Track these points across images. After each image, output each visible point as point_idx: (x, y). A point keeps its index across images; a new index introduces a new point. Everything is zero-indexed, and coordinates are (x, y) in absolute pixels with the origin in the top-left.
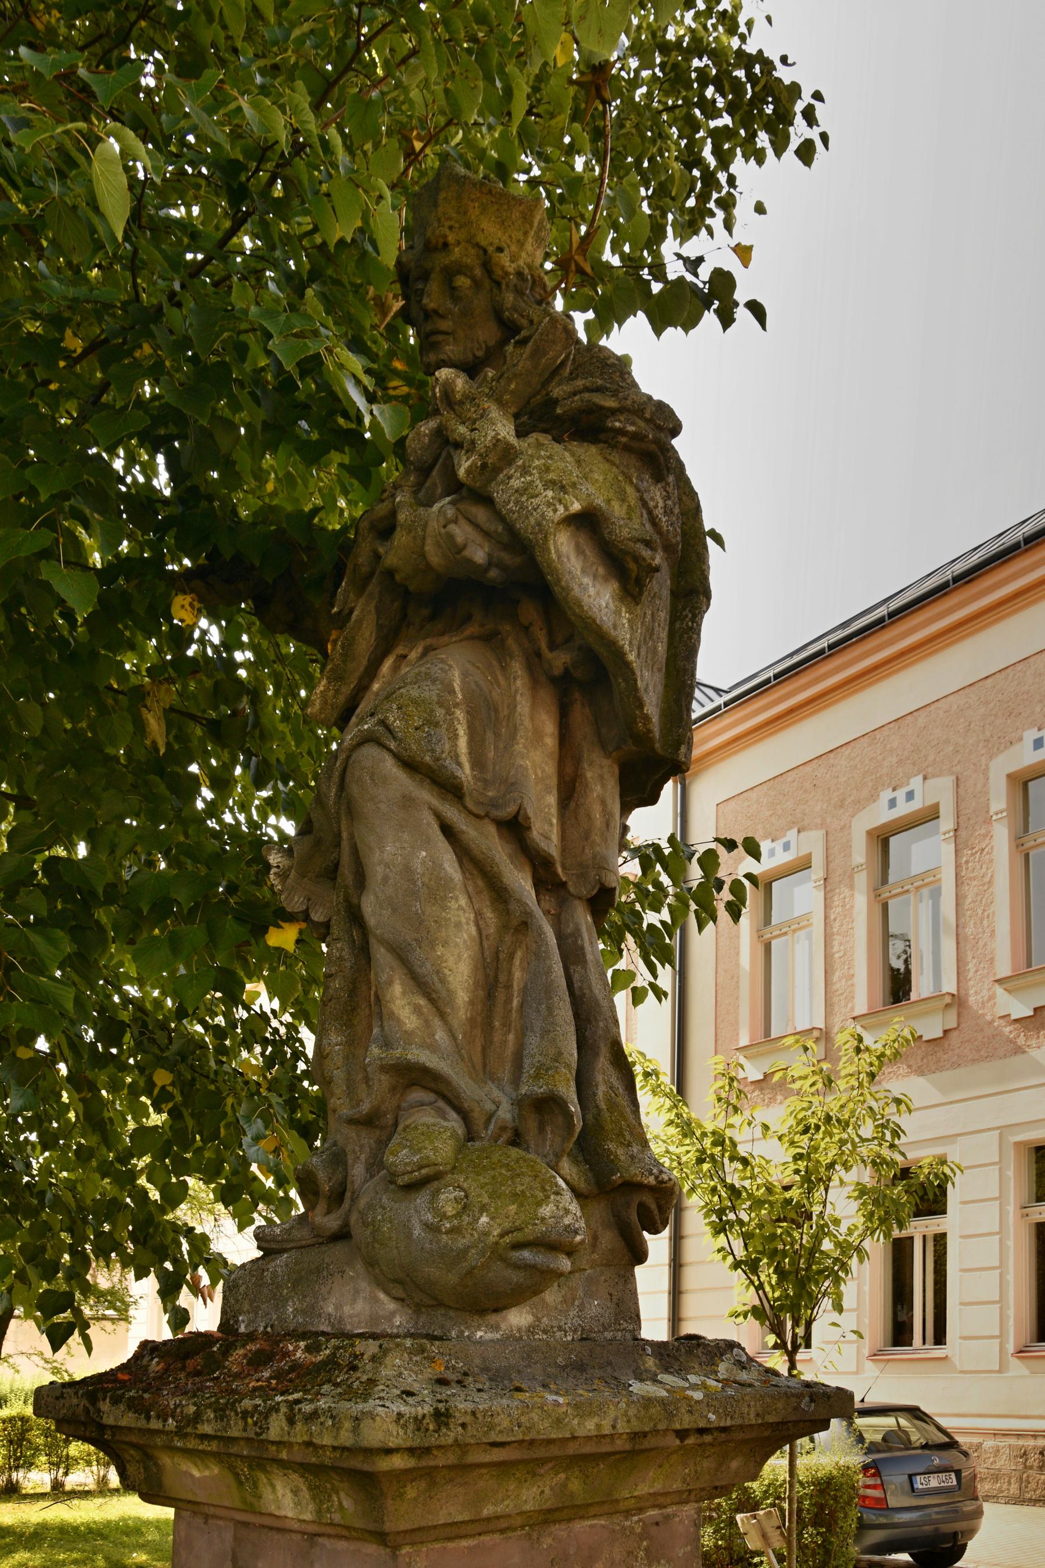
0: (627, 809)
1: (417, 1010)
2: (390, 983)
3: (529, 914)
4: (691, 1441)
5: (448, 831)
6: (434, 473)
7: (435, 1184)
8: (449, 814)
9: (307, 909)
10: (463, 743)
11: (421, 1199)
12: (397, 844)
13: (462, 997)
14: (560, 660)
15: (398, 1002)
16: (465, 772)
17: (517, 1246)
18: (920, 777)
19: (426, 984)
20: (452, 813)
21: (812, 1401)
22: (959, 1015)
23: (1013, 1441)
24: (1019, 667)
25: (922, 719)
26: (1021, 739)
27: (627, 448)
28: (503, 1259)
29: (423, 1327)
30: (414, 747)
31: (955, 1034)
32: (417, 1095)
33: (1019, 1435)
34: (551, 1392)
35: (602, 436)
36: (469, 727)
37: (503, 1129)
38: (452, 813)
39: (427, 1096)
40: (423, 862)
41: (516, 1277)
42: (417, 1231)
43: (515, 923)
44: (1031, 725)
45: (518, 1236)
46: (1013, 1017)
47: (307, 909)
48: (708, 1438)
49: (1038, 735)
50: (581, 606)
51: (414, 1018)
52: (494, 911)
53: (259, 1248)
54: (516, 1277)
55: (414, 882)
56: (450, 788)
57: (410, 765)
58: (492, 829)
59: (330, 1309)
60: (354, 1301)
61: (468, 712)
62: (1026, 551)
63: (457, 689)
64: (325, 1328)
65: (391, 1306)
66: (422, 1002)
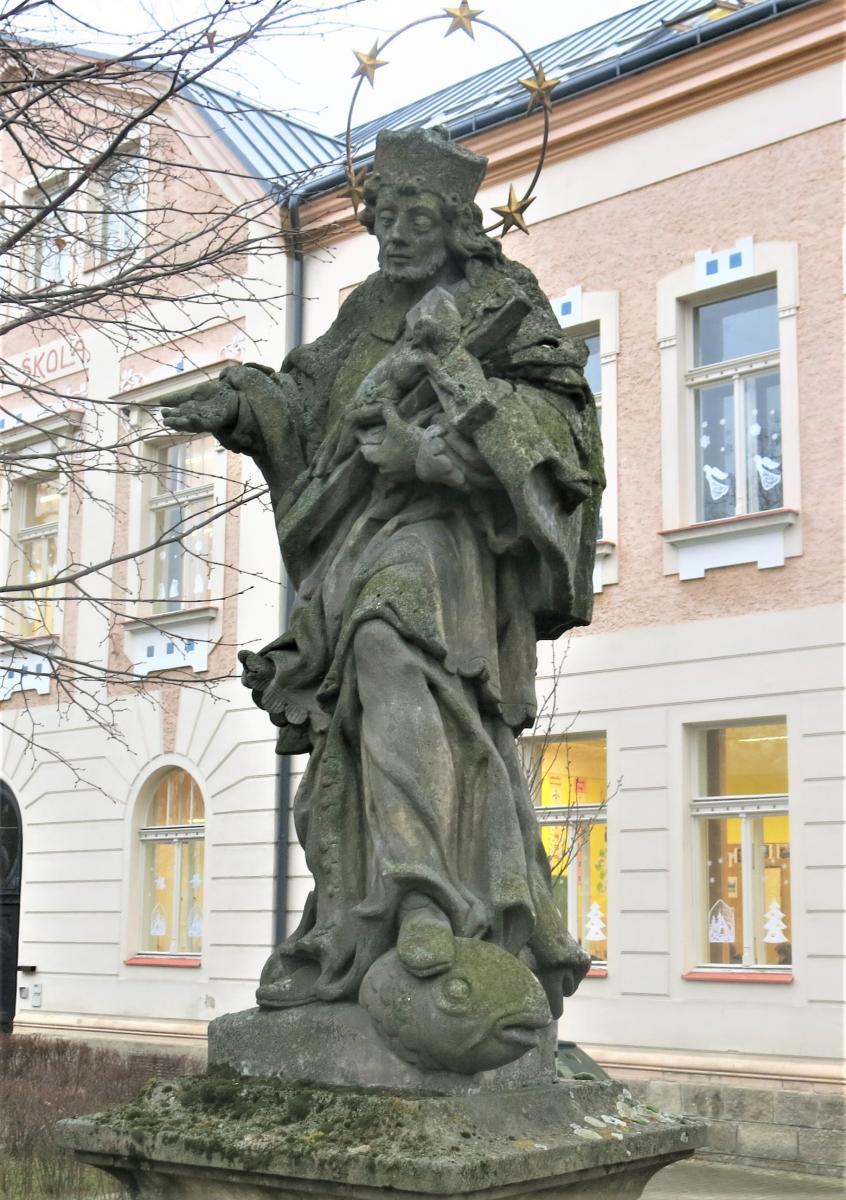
0: (538, 640)
1: (417, 832)
2: (396, 810)
3: (489, 752)
4: (612, 1171)
5: (433, 687)
6: (414, 392)
7: (445, 977)
8: (436, 677)
9: (284, 712)
10: (439, 615)
11: (436, 988)
12: (401, 702)
13: (447, 820)
14: (502, 543)
15: (404, 826)
16: (441, 640)
17: (508, 1027)
18: (578, 288)
19: (426, 814)
20: (437, 675)
21: (687, 1135)
22: (620, 568)
23: (683, 1080)
24: (694, 176)
25: (581, 219)
26: (692, 260)
27: (561, 393)
28: (497, 1037)
29: (430, 1084)
30: (415, 628)
31: (616, 590)
32: (416, 899)
33: (691, 1071)
34: (538, 1142)
35: (547, 384)
36: (443, 601)
37: (480, 927)
38: (437, 675)
39: (425, 901)
40: (419, 717)
41: (502, 1049)
42: (434, 1014)
43: (478, 757)
44: (705, 246)
45: (511, 1020)
46: (682, 578)
47: (284, 712)
48: (622, 1169)
49: (711, 258)
50: (540, 530)
51: (415, 839)
52: (459, 746)
53: (258, 1003)
54: (502, 1049)
55: (412, 731)
56: (435, 656)
57: (410, 640)
58: (458, 682)
59: (343, 1065)
60: (367, 1059)
61: (441, 588)
62: (703, 48)
63: (433, 568)
64: (338, 1081)
65: (402, 1067)
66: (420, 826)
